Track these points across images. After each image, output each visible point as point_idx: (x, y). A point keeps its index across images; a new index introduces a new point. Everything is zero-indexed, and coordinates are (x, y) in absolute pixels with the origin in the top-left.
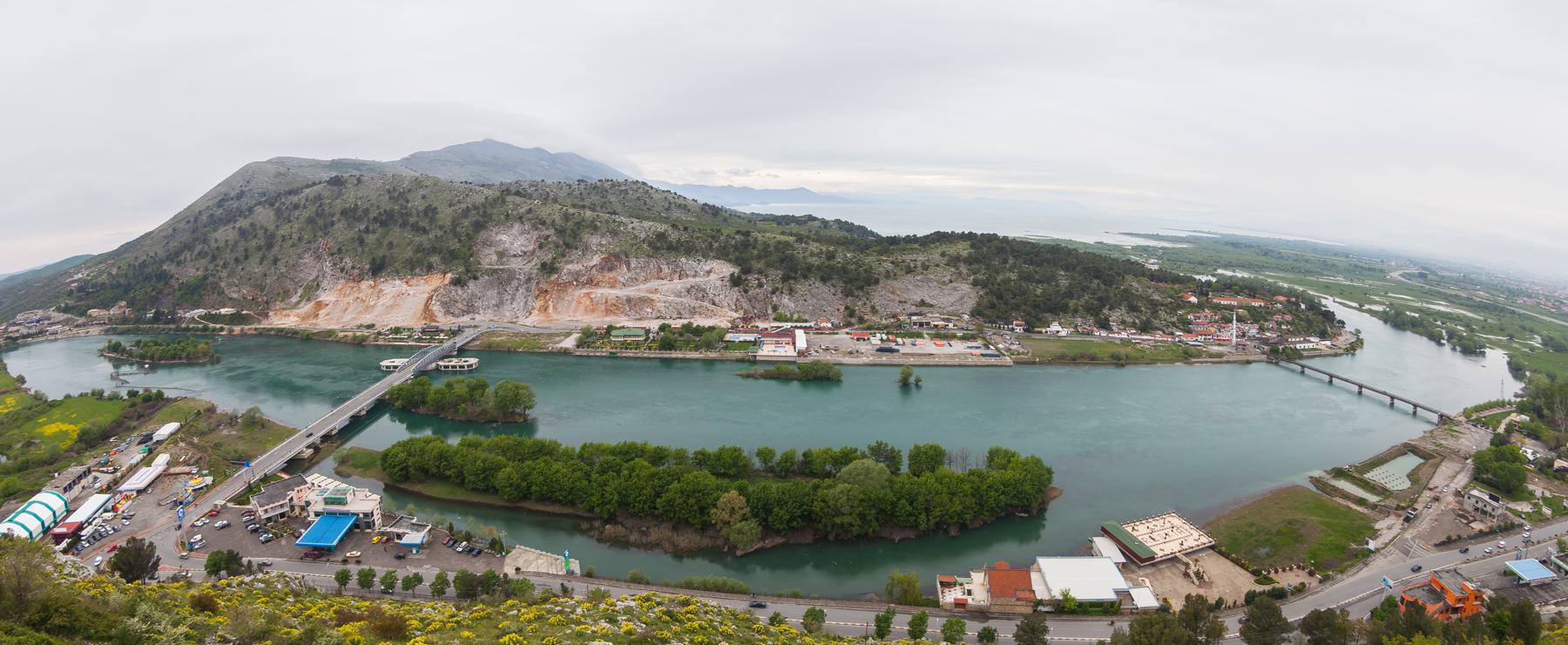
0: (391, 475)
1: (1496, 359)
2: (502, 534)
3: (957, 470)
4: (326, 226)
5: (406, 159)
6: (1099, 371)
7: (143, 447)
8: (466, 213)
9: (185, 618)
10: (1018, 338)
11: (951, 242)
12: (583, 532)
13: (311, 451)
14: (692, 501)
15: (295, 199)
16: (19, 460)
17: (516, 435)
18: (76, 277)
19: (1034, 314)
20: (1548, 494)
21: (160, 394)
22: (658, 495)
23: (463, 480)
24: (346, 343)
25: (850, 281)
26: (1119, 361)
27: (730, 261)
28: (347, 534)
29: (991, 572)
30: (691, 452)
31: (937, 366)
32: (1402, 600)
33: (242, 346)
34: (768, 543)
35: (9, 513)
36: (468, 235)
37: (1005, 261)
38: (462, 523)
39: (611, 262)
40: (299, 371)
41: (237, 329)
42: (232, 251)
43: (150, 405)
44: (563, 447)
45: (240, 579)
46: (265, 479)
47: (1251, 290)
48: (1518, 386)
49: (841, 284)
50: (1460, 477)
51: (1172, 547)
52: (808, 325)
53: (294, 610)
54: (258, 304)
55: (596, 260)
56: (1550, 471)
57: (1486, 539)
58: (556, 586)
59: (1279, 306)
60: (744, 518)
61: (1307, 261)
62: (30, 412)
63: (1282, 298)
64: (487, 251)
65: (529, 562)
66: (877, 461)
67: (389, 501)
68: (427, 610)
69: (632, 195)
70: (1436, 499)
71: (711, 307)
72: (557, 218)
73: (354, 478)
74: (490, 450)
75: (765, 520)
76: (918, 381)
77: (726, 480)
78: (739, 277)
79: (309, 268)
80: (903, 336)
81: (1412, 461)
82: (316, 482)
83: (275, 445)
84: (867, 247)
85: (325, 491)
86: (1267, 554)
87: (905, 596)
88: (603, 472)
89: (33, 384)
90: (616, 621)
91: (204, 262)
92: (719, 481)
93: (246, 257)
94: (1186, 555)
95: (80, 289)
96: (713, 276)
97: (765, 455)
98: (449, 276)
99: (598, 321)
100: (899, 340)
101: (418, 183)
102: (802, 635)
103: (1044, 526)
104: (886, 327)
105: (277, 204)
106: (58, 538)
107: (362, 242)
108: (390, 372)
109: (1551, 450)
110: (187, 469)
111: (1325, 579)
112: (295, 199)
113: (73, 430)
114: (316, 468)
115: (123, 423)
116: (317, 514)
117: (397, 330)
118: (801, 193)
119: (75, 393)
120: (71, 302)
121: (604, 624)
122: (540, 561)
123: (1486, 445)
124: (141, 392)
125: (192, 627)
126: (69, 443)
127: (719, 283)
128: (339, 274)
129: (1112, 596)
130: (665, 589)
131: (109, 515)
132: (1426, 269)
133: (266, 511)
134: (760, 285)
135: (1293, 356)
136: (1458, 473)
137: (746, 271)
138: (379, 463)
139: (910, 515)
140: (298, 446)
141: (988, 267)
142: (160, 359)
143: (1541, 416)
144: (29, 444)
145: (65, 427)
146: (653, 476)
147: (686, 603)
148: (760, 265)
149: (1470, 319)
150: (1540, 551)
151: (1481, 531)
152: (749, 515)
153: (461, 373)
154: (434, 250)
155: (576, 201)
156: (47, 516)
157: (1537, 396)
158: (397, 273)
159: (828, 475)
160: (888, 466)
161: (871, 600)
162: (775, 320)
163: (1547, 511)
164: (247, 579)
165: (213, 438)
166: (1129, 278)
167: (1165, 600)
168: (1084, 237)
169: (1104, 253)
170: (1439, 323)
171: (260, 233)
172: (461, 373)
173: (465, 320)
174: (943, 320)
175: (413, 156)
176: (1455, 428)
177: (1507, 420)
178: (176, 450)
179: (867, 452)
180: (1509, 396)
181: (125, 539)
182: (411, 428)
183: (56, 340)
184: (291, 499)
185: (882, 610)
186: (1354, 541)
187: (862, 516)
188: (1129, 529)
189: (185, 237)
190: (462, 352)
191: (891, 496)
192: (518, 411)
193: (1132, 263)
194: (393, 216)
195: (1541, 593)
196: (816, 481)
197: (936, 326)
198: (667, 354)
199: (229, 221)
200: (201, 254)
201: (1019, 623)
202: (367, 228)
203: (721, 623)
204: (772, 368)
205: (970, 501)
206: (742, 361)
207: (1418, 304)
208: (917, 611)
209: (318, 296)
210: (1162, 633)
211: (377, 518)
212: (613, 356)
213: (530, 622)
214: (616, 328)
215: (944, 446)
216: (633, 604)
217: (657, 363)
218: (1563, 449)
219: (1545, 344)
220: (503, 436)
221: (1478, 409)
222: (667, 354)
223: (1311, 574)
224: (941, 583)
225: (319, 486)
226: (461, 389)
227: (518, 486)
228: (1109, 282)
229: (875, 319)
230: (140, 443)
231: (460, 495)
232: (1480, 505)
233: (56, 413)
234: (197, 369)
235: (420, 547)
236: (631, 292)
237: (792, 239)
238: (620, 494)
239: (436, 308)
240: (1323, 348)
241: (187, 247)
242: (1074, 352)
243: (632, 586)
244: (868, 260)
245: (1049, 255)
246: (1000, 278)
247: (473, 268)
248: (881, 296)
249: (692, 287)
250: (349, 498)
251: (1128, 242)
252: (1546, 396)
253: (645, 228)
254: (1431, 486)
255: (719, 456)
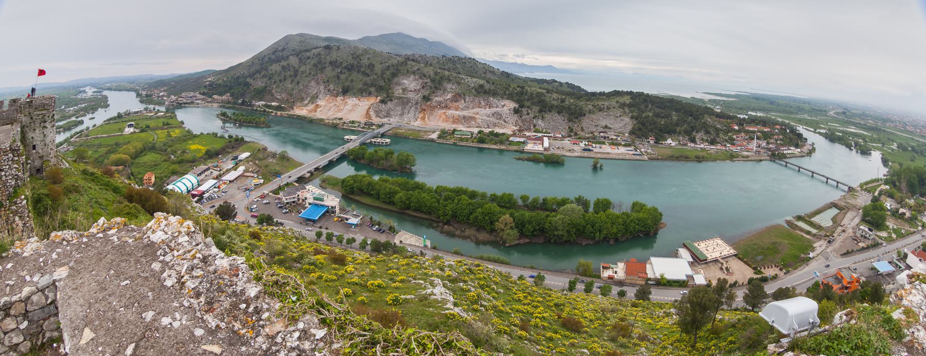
0: (345, 190)
1: (876, 155)
2: (395, 224)
3: (616, 211)
4: (322, 69)
5: (361, 39)
6: (689, 164)
7: (233, 161)
8: (388, 68)
9: (246, 240)
10: (651, 146)
11: (621, 96)
12: (434, 228)
13: (309, 174)
14: (487, 218)
15: (308, 54)
16: (179, 158)
17: (406, 178)
18: (208, 80)
19: (659, 134)
20: (895, 227)
21: (242, 139)
22: (471, 214)
23: (379, 197)
24: (329, 125)
25: (572, 114)
26: (699, 159)
27: (514, 101)
28: (322, 215)
29: (628, 264)
30: (489, 194)
31: (611, 159)
32: (823, 282)
33: (280, 121)
34: (522, 241)
35: (174, 181)
36: (388, 79)
37: (647, 106)
38: (377, 217)
39: (457, 97)
40: (303, 136)
41: (279, 113)
42: (278, 76)
43: (238, 143)
44: (428, 186)
45: (272, 227)
46: (287, 185)
47: (764, 122)
48: (885, 170)
49: (567, 115)
50: (856, 219)
51: (716, 255)
52: (550, 135)
53: (295, 245)
54: (289, 103)
55: (449, 96)
56: (897, 215)
57: (865, 251)
58: (418, 251)
59: (777, 131)
60: (511, 228)
61: (791, 107)
62: (185, 138)
63: (778, 127)
64: (397, 88)
65: (406, 239)
66: (578, 205)
67: (343, 202)
68: (356, 254)
69: (468, 65)
70: (844, 231)
71: (504, 123)
72: (432, 73)
73: (328, 189)
74: (393, 184)
75: (522, 230)
76: (601, 166)
77: (505, 209)
78: (518, 109)
79: (313, 88)
80: (596, 143)
81: (834, 211)
82: (310, 189)
83: (293, 169)
84: (581, 97)
85: (314, 194)
86: (761, 259)
87: (585, 272)
88: (446, 200)
89: (188, 125)
90: (444, 270)
91: (266, 79)
92: (501, 209)
93: (285, 80)
94: (722, 259)
95: (210, 85)
96: (505, 108)
97: (525, 198)
98: (379, 98)
99: (449, 126)
100: (594, 145)
101: (366, 51)
102: (532, 286)
103: (655, 242)
104: (588, 138)
105: (300, 56)
106: (194, 196)
107: (338, 78)
108: (348, 142)
109: (898, 203)
110: (252, 175)
111: (787, 272)
112: (308, 54)
113: (204, 149)
114: (311, 183)
115: (225, 149)
116: (310, 204)
117: (353, 122)
118: (550, 68)
119: (205, 133)
120: (206, 91)
121: (438, 271)
122: (412, 239)
123: (869, 202)
124: (234, 137)
125: (249, 244)
126: (201, 154)
127: (508, 112)
128: (327, 92)
129: (684, 278)
130: (470, 259)
131: (216, 190)
132: (846, 110)
133: (286, 199)
134: (528, 114)
135: (782, 157)
136: (855, 217)
137: (522, 106)
138: (340, 184)
139: (592, 233)
140: (303, 171)
141: (639, 109)
142: (244, 122)
143: (895, 186)
144: (184, 152)
145: (200, 147)
146: (470, 204)
147: (478, 266)
148: (528, 104)
149: (865, 136)
150: (887, 256)
151: (863, 247)
152: (514, 227)
153: (382, 146)
154: (372, 85)
155: (441, 66)
156: (189, 185)
157: (893, 175)
158: (355, 95)
159: (554, 210)
160: (583, 208)
161: (568, 273)
162: (534, 132)
163: (894, 236)
164: (275, 228)
165: (265, 162)
166: (706, 116)
167: (710, 281)
168: (686, 94)
169: (695, 103)
170: (851, 138)
171: (292, 69)
172: (382, 146)
173: (385, 120)
174: (616, 136)
175: (364, 38)
176: (855, 194)
177: (879, 189)
178: (248, 165)
179: (574, 200)
180: (881, 176)
181: (223, 201)
182: (357, 170)
183: (198, 107)
184: (299, 195)
185: (573, 278)
186: (803, 253)
187: (568, 232)
188: (696, 245)
189: (257, 67)
190: (383, 135)
191: (583, 223)
192: (408, 167)
193: (708, 108)
194: (353, 67)
195: (887, 278)
196: (547, 213)
197: (612, 139)
198: (481, 146)
199: (277, 62)
200: (264, 76)
201: (638, 289)
202: (341, 71)
203: (494, 277)
204: (531, 156)
205: (621, 227)
206: (517, 151)
207: (842, 129)
208: (589, 280)
209: (317, 102)
210: (704, 297)
211: (337, 209)
212: (455, 144)
213: (403, 265)
214: (457, 131)
215: (611, 200)
216: (453, 263)
217: (476, 150)
218: (904, 203)
219: (898, 147)
220: (400, 178)
221: (867, 183)
222: (481, 146)
223: (781, 270)
224: (603, 267)
225: (311, 191)
226: (381, 154)
227: (405, 203)
228: (696, 119)
229: (583, 134)
230: (232, 160)
231: (377, 204)
232: (864, 234)
233: (197, 140)
234: (259, 129)
235: (356, 225)
236: (465, 113)
237: (544, 91)
238: (453, 211)
239: (372, 113)
240: (797, 153)
241: (258, 72)
242: (678, 154)
243: (455, 255)
244: (581, 103)
245: (668, 104)
246: (644, 115)
247: (391, 95)
248: (586, 122)
249: (495, 113)
250: (325, 198)
251: (707, 97)
252: (898, 175)
253: (473, 82)
254: (842, 224)
255: (502, 197)
